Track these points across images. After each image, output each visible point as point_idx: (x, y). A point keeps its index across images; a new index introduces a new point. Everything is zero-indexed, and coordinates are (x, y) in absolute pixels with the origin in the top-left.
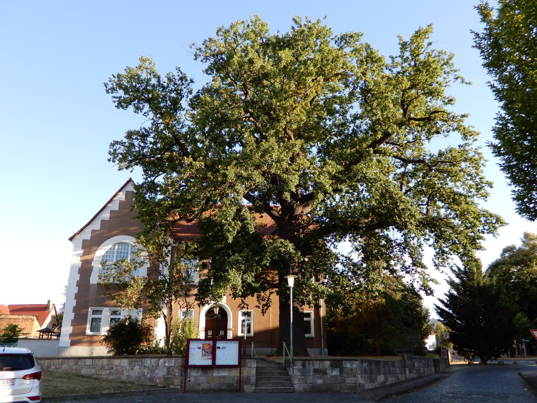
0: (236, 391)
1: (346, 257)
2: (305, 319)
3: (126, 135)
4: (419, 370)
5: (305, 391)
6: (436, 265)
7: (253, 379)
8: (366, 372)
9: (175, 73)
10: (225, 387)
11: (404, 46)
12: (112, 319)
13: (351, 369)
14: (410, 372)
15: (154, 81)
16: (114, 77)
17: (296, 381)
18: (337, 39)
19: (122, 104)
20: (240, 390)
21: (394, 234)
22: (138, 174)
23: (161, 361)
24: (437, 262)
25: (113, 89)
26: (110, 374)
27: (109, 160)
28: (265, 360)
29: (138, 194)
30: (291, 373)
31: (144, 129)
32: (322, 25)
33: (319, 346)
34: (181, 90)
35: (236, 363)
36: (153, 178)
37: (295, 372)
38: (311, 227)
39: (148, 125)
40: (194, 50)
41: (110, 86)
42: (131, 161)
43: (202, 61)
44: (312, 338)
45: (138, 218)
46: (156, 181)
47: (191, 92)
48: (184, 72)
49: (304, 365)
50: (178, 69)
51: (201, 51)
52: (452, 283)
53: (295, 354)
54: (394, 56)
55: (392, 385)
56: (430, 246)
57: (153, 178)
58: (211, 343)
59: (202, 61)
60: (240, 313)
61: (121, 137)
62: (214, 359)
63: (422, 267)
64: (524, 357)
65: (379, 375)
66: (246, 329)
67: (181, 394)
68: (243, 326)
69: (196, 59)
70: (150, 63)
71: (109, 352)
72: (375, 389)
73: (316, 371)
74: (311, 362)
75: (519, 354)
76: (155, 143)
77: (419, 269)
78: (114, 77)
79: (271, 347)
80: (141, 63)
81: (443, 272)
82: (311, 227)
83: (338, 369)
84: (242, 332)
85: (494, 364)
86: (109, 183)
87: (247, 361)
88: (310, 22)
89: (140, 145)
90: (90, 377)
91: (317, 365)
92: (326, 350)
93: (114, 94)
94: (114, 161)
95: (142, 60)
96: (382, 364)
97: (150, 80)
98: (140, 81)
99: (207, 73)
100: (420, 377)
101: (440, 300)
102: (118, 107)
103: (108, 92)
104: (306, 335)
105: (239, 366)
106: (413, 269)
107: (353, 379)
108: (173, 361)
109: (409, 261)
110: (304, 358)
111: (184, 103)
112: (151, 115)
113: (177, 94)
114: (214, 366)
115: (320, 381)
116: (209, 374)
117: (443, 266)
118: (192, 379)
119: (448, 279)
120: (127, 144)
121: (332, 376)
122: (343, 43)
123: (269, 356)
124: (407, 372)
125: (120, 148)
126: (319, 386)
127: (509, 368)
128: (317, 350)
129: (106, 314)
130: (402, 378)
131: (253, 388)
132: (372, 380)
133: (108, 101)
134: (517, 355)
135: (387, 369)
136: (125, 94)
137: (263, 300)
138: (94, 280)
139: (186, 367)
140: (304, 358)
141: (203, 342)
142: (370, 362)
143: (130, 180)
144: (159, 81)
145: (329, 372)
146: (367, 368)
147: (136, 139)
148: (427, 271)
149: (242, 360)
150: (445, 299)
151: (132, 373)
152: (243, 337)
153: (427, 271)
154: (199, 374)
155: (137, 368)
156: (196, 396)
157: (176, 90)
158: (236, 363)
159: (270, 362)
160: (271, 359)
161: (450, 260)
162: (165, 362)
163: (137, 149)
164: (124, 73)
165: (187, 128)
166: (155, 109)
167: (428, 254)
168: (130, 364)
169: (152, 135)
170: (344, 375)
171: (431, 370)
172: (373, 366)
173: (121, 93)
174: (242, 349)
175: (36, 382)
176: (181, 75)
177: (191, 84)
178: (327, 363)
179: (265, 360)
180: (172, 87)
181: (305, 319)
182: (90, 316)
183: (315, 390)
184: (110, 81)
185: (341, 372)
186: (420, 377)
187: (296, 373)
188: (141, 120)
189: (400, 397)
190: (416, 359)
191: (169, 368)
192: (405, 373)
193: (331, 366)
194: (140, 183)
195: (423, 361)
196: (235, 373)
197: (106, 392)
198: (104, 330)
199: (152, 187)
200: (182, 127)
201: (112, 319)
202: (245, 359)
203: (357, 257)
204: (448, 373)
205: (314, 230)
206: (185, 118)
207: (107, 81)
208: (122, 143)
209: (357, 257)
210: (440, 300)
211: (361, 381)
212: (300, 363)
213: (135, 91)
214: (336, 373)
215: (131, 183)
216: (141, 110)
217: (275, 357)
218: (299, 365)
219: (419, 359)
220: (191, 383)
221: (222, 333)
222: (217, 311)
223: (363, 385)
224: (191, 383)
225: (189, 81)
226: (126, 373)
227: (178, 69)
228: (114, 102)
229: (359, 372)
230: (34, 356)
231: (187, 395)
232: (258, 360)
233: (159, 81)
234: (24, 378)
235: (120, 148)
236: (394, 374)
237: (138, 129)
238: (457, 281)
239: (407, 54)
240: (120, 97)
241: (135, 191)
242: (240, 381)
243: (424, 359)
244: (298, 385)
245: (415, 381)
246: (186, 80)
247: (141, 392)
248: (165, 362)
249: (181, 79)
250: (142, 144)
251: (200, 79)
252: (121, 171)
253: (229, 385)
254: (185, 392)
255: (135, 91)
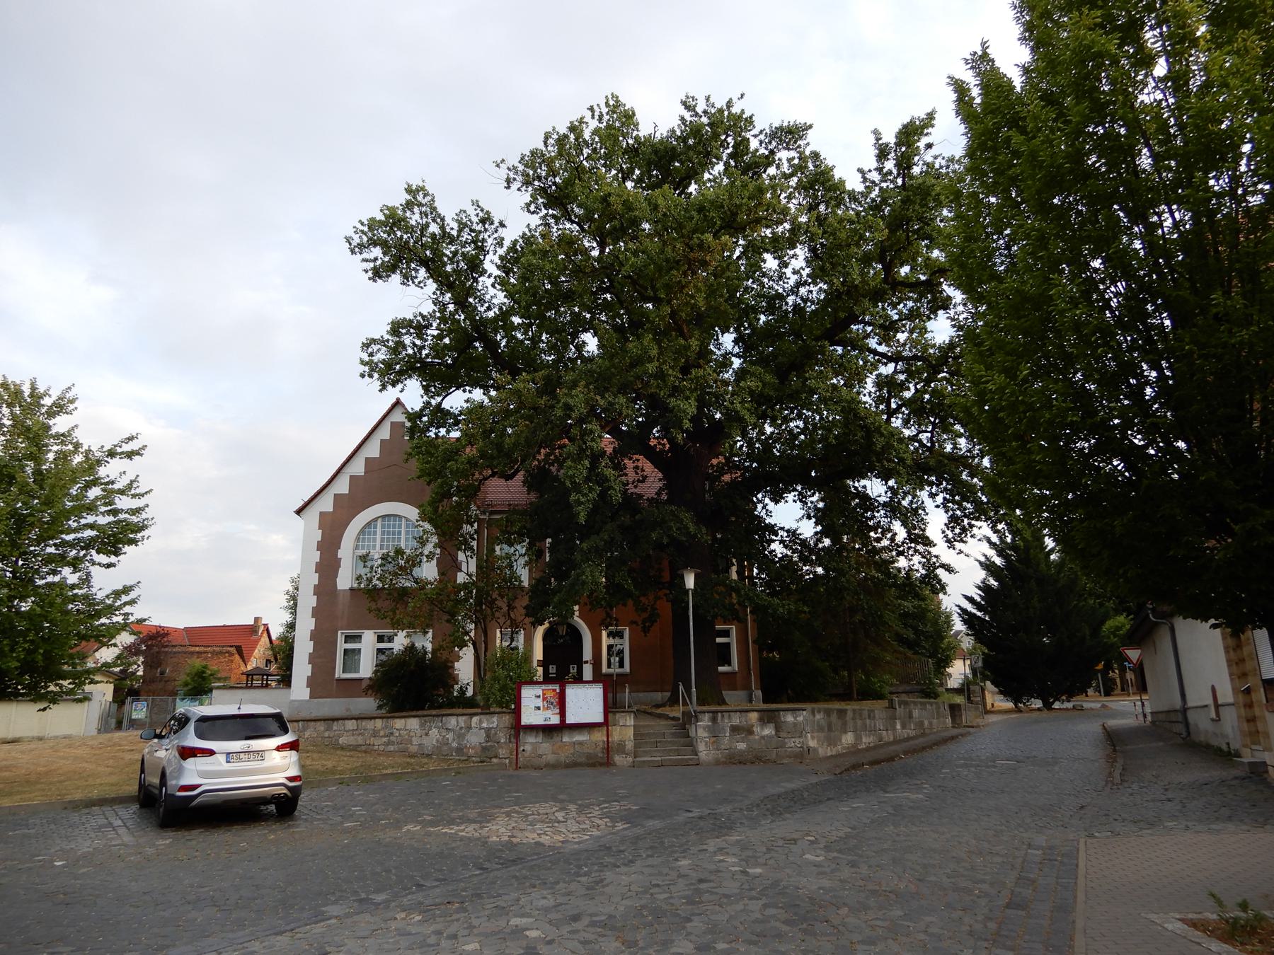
0: (601, 764)
1: (788, 531)
2: (719, 640)
3: (388, 328)
4: (922, 723)
5: (717, 763)
6: (948, 541)
7: (630, 745)
8: (821, 729)
9: (472, 211)
10: (583, 760)
11: (882, 154)
12: (380, 651)
13: (795, 725)
14: (903, 727)
15: (434, 228)
16: (362, 224)
17: (701, 747)
18: (762, 137)
19: (378, 273)
20: (608, 763)
21: (875, 488)
22: (412, 394)
23: (475, 719)
24: (950, 535)
25: (361, 246)
26: (389, 743)
27: (363, 376)
28: (650, 714)
29: (413, 431)
30: (692, 733)
31: (421, 314)
32: (736, 110)
33: (747, 687)
34: (484, 240)
35: (600, 719)
36: (439, 399)
37: (701, 730)
38: (727, 478)
39: (428, 308)
40: (503, 173)
41: (356, 240)
42: (401, 373)
43: (519, 189)
44: (733, 674)
45: (419, 477)
46: (446, 405)
47: (500, 243)
48: (486, 209)
49: (714, 720)
50: (476, 204)
51: (516, 173)
52: (988, 566)
53: (701, 702)
54: (866, 169)
55: (868, 749)
56: (937, 506)
57: (439, 399)
58: (557, 687)
59: (519, 189)
60: (604, 634)
61: (382, 331)
62: (563, 714)
63: (925, 545)
64: (1129, 695)
65: (846, 732)
66: (615, 660)
67: (511, 772)
68: (610, 655)
69: (508, 187)
70: (425, 195)
71: (380, 707)
72: (839, 755)
73: (734, 729)
74: (726, 715)
75: (1123, 689)
76: (440, 337)
77: (920, 547)
78: (362, 224)
79: (662, 691)
80: (409, 197)
81: (961, 552)
82: (727, 478)
83: (772, 725)
84: (609, 666)
85: (1067, 709)
86: (360, 410)
87: (618, 715)
88: (713, 106)
89: (414, 344)
90: (355, 748)
91: (736, 720)
92: (759, 693)
93: (365, 255)
94: (371, 376)
95: (409, 190)
96: (850, 714)
97: (427, 225)
98: (409, 229)
99: (529, 211)
100: (923, 735)
101: (966, 597)
102: (373, 279)
103: (353, 252)
104: (721, 669)
105: (606, 723)
106: (909, 548)
107: (797, 740)
108: (495, 719)
109: (901, 533)
110: (713, 708)
111: (491, 264)
112: (432, 286)
113: (477, 248)
114: (563, 727)
115: (742, 746)
116: (556, 739)
117: (962, 541)
118: (528, 748)
119: (983, 559)
120: (391, 343)
121: (763, 737)
122: (774, 143)
123: (658, 706)
124: (898, 727)
125: (379, 350)
126: (741, 753)
127: (1092, 714)
128: (742, 694)
129: (368, 642)
130: (888, 736)
131: (630, 759)
132: (832, 742)
133: (356, 267)
134: (1118, 690)
135: (859, 722)
136: (385, 254)
137: (645, 610)
138: (345, 581)
139: (518, 729)
140: (713, 708)
141: (544, 687)
142: (828, 712)
143: (398, 403)
144: (442, 227)
145: (757, 729)
146: (823, 723)
147: (408, 333)
148: (934, 551)
149: (610, 715)
150: (976, 594)
151: (425, 741)
152: (611, 675)
153: (934, 551)
154: (540, 739)
155: (434, 732)
156: (535, 774)
157: (474, 242)
158: (600, 719)
159: (660, 716)
160: (659, 711)
161: (975, 531)
162: (481, 722)
163: (410, 351)
164: (381, 217)
165: (496, 310)
166: (435, 271)
167: (936, 521)
168: (422, 725)
169: (435, 325)
170: (782, 734)
171: (945, 723)
172: (834, 718)
173: (377, 252)
174: (610, 695)
175: (292, 756)
176: (481, 214)
177: (500, 229)
178: (754, 716)
179: (650, 714)
180: (466, 236)
181: (719, 640)
182: (341, 645)
183: (734, 760)
184: (356, 232)
185: (777, 729)
186: (923, 735)
187: (702, 733)
188: (416, 298)
189: (876, 767)
190: (915, 703)
191: (488, 730)
192: (894, 729)
193: (761, 720)
194: (417, 408)
195: (928, 706)
196: (599, 736)
197: (389, 771)
198: (366, 669)
199: (440, 416)
200: (489, 309)
201: (380, 651)
202: (614, 713)
203: (808, 529)
204: (978, 726)
205: (733, 481)
206: (492, 295)
207: (351, 233)
208: (383, 342)
209: (808, 529)
210: (966, 597)
211: (812, 744)
212: (707, 716)
213: (401, 243)
214: (768, 731)
215: (398, 411)
216: (413, 278)
217: (668, 708)
218: (705, 721)
219: (921, 703)
220: (526, 754)
221: (573, 670)
222: (562, 630)
223: (815, 750)
224: (526, 754)
225: (496, 224)
226: (415, 741)
227: (476, 204)
228: (366, 271)
229: (808, 728)
230: (285, 716)
231: (522, 772)
232: (637, 714)
233: (442, 227)
234: (279, 749)
235: (379, 350)
236: (872, 731)
237: (409, 316)
238: (998, 561)
239: (890, 165)
240: (376, 259)
241: (408, 424)
242: (608, 749)
243: (931, 704)
244: (705, 752)
245: (912, 742)
246: (492, 223)
247: (446, 770)
248: (481, 722)
249: (483, 221)
250: (418, 342)
251: (517, 218)
252: (384, 392)
253: (589, 756)
254: (517, 768)
255: (401, 243)
